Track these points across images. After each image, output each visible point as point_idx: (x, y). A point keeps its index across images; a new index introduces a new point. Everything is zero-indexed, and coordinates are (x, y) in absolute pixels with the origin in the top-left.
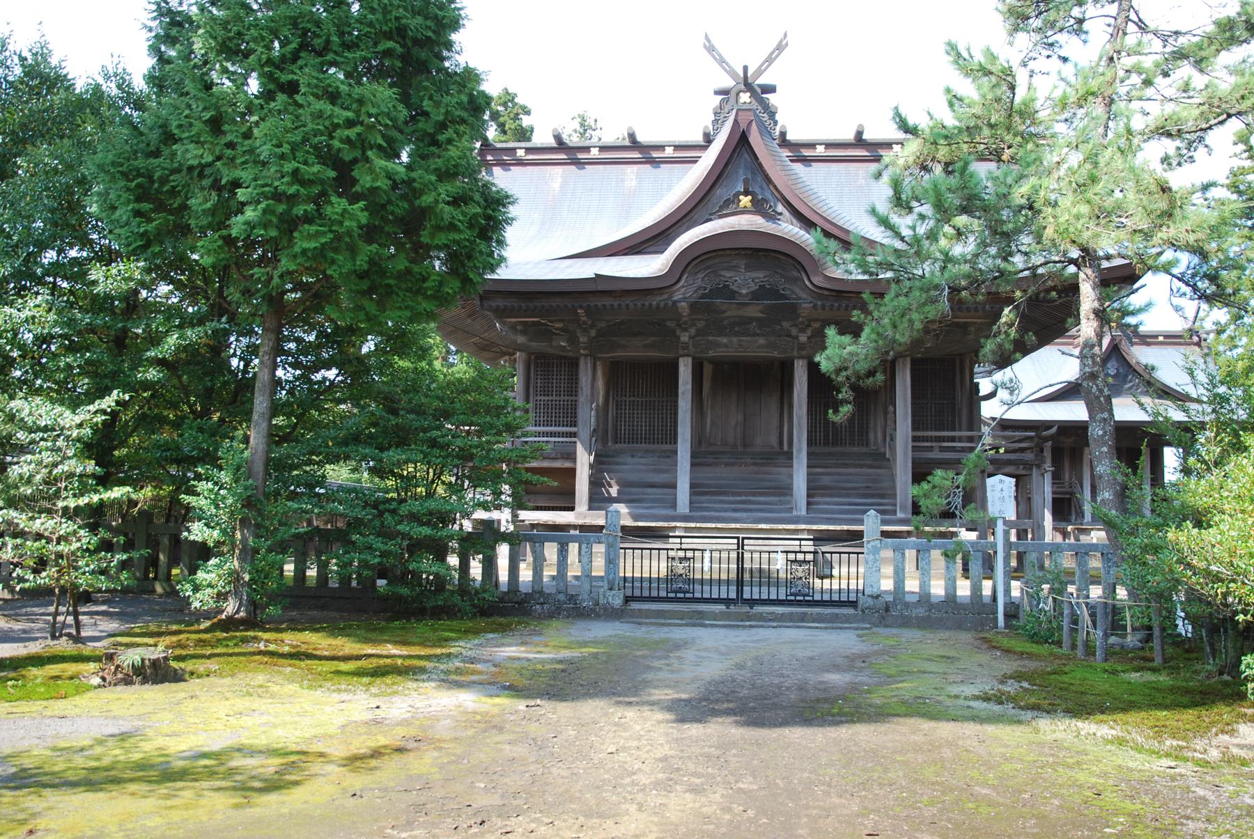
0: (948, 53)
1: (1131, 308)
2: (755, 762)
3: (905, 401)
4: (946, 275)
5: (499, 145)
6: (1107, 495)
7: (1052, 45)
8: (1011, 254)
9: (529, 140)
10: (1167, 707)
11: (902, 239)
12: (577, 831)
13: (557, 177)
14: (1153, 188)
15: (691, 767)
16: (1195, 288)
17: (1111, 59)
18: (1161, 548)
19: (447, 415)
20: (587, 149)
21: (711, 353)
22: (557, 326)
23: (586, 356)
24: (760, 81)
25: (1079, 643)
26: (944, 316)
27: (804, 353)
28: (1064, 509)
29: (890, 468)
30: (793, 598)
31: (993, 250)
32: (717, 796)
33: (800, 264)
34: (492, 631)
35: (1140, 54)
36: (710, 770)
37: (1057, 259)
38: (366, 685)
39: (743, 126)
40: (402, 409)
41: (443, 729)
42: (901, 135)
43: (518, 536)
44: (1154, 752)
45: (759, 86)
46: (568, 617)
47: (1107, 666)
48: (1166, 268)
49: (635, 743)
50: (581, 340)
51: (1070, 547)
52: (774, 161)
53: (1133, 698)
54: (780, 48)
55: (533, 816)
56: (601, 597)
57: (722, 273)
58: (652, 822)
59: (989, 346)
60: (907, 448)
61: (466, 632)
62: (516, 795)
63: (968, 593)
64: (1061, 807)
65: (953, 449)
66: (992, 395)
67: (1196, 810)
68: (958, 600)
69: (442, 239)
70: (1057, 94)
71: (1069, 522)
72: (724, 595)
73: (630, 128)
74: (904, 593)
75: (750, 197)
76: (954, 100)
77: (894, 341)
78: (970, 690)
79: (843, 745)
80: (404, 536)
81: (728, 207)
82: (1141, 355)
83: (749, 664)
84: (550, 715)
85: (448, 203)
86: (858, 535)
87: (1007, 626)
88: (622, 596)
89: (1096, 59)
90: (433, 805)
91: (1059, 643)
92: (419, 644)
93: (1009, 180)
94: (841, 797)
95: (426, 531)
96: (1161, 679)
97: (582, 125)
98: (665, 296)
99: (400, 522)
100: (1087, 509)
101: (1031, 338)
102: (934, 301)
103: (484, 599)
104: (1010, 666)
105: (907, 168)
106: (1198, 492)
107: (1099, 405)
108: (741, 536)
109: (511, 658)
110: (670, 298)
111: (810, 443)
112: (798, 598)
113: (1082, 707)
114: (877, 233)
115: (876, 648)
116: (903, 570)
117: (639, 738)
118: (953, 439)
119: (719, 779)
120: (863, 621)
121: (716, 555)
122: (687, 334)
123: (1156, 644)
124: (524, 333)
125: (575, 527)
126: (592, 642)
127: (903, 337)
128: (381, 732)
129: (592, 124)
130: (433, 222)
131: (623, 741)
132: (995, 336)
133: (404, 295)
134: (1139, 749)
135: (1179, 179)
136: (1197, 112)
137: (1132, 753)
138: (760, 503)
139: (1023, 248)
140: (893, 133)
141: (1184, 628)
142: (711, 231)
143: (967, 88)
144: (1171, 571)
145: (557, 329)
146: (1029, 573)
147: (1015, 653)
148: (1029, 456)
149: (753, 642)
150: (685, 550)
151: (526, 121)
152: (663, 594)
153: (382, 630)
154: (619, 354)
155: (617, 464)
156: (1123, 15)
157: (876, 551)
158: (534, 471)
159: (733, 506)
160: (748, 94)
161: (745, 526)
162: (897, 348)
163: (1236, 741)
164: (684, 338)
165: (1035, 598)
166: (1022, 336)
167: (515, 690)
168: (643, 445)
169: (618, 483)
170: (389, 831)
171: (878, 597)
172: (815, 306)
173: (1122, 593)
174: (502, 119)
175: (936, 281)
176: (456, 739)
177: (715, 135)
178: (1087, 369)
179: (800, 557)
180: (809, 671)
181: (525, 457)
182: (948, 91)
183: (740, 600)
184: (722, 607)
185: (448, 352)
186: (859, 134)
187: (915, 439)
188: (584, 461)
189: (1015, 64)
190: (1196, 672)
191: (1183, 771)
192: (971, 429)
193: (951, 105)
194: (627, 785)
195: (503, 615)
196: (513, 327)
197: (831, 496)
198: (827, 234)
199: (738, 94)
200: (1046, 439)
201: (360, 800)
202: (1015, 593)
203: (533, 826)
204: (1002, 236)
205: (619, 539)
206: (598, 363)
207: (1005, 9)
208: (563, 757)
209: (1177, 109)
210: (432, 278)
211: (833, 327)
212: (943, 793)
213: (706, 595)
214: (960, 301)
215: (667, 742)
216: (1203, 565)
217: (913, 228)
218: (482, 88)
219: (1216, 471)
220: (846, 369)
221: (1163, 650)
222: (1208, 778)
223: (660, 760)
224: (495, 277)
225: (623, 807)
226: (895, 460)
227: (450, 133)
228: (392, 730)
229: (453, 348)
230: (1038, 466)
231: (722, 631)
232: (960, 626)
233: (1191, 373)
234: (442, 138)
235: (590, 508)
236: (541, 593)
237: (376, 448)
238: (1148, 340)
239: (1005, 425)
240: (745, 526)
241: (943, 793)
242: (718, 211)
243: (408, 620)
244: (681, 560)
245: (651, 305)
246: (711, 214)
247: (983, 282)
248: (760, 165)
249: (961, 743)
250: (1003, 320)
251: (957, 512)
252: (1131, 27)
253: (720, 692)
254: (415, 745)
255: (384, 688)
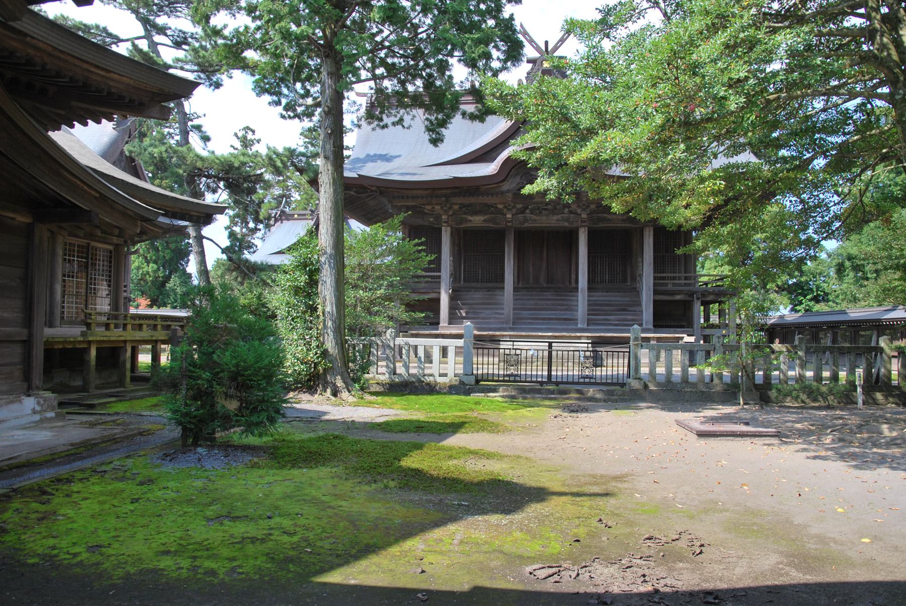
150: (516, 349)
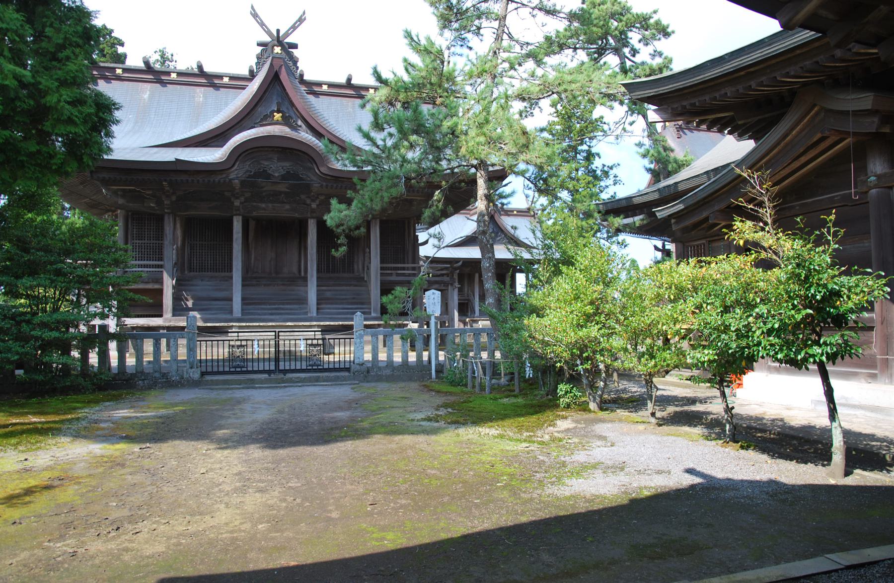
0: (406, 37)
1: (504, 194)
2: (298, 469)
3: (376, 245)
4: (403, 170)
5: (102, 65)
6: (491, 300)
7: (464, 39)
8: (440, 160)
9: (123, 62)
10: (523, 416)
11: (378, 147)
12: (186, 526)
13: (146, 91)
14: (519, 132)
15: (257, 476)
16: (535, 185)
17: (495, 52)
18: (520, 329)
19: (68, 253)
20: (168, 73)
21: (255, 214)
22: (147, 192)
23: (169, 213)
24: (288, 40)
25: (477, 384)
26: (402, 195)
27: (314, 215)
28: (465, 309)
29: (367, 286)
30: (233, 370)
31: (431, 157)
32: (276, 493)
33: (314, 160)
34: (109, 401)
35: (509, 52)
36: (269, 477)
37: (465, 164)
38: (14, 445)
39: (276, 68)
40: (33, 248)
41: (79, 470)
42: (379, 84)
43: (125, 335)
44: (518, 440)
45: (287, 43)
46: (162, 388)
47: (491, 396)
48: (522, 173)
49: (218, 466)
50: (165, 202)
51: (471, 331)
52: (298, 94)
53: (506, 412)
54: (301, 20)
55: (154, 519)
56: (185, 373)
57: (262, 162)
58: (236, 513)
59: (427, 213)
60: (377, 274)
61: (89, 402)
62: (139, 508)
63: (400, 360)
64: (474, 475)
65: (403, 275)
66: (426, 242)
67: (540, 467)
68: (409, 364)
69: (62, 129)
70: (467, 68)
71: (467, 316)
72: (267, 368)
73: (199, 62)
74: (378, 361)
75: (281, 114)
76: (409, 66)
77: (372, 209)
78: (420, 416)
79: (350, 454)
80: (37, 339)
81: (266, 120)
82: (508, 222)
83: (287, 410)
84: (157, 453)
85: (69, 103)
86: (351, 327)
87: (437, 377)
88: (199, 372)
89: (487, 51)
90: (79, 522)
91: (466, 385)
92: (53, 413)
93: (441, 117)
94: (352, 484)
95: (55, 334)
96: (519, 400)
97: (162, 57)
98: (224, 176)
99: (34, 329)
100: (477, 309)
101: (450, 209)
102: (395, 185)
103: (101, 378)
104: (440, 400)
105: (381, 103)
106: (537, 298)
107: (487, 250)
108: (277, 330)
109: (124, 418)
110: (227, 177)
111: (318, 271)
112: (314, 368)
113: (479, 419)
114: (360, 142)
115: (363, 395)
116: (377, 348)
117: (221, 462)
118: (404, 269)
119: (276, 482)
120: (354, 379)
121: (261, 343)
122: (239, 201)
123: (516, 380)
124: (123, 196)
125: (163, 328)
126: (181, 403)
127: (377, 207)
128: (31, 477)
129: (170, 57)
130: (55, 116)
131: (210, 465)
132: (430, 207)
133: (35, 169)
134: (510, 439)
135: (530, 124)
136: (538, 89)
137: (508, 442)
138: (287, 309)
139: (447, 157)
140: (371, 81)
141: (529, 373)
142: (255, 135)
143: (416, 59)
144: (526, 342)
145: (148, 195)
146: (449, 346)
147: (443, 392)
148: (446, 279)
149: (287, 396)
150: (241, 340)
151: (120, 50)
152: (227, 369)
153: (23, 406)
154: (193, 213)
155: (193, 285)
156: (501, 29)
157: (361, 337)
158: (136, 291)
159: (270, 311)
160: (280, 48)
161: (278, 324)
162: (375, 213)
163: (556, 429)
164: (237, 203)
165: (452, 360)
166: (445, 208)
167: (129, 439)
168: (209, 273)
169: (192, 298)
170: (46, 544)
171: (362, 364)
172: (322, 186)
173: (498, 355)
174: (101, 46)
175: (398, 173)
176: (90, 475)
177: (258, 72)
178: (481, 229)
179: (315, 342)
180: (324, 412)
181: (129, 282)
182: (405, 60)
183: (277, 370)
184: (266, 376)
185: (64, 208)
186: (349, 80)
187: (382, 269)
188: (168, 284)
189: (444, 48)
190: (536, 395)
191: (533, 448)
192: (414, 262)
193: (407, 70)
194: (217, 492)
195: (114, 389)
196: (115, 192)
197: (332, 304)
198: (331, 142)
199: (273, 47)
200: (456, 269)
201: (20, 526)
202: (442, 358)
203: (155, 526)
204: (435, 149)
205: (196, 335)
206: (177, 218)
207: (439, 14)
208: (170, 479)
209: (529, 86)
210: (59, 156)
211: (335, 199)
212: (410, 475)
213: (256, 369)
214: (411, 187)
215: (239, 463)
216: (541, 337)
217: (384, 140)
218: (93, 23)
219: (547, 286)
220: (342, 225)
221: (519, 385)
222: (545, 450)
223: (236, 474)
224: (110, 157)
225: (215, 506)
226: (370, 281)
227: (67, 52)
228: (39, 474)
229: (67, 205)
230: (452, 285)
231: (267, 391)
232: (410, 379)
233: (534, 232)
234: (61, 55)
235: (174, 315)
236: (142, 372)
237: (12, 276)
238: (509, 213)
239: (435, 261)
240: (278, 324)
241: (410, 475)
242: (260, 122)
243: (43, 396)
244: (239, 347)
245: (214, 181)
246: (255, 124)
247: (424, 175)
248: (287, 94)
249: (417, 446)
250: (435, 198)
251: (409, 312)
252: (505, 37)
253: (270, 429)
254: (59, 482)
255: (29, 446)
